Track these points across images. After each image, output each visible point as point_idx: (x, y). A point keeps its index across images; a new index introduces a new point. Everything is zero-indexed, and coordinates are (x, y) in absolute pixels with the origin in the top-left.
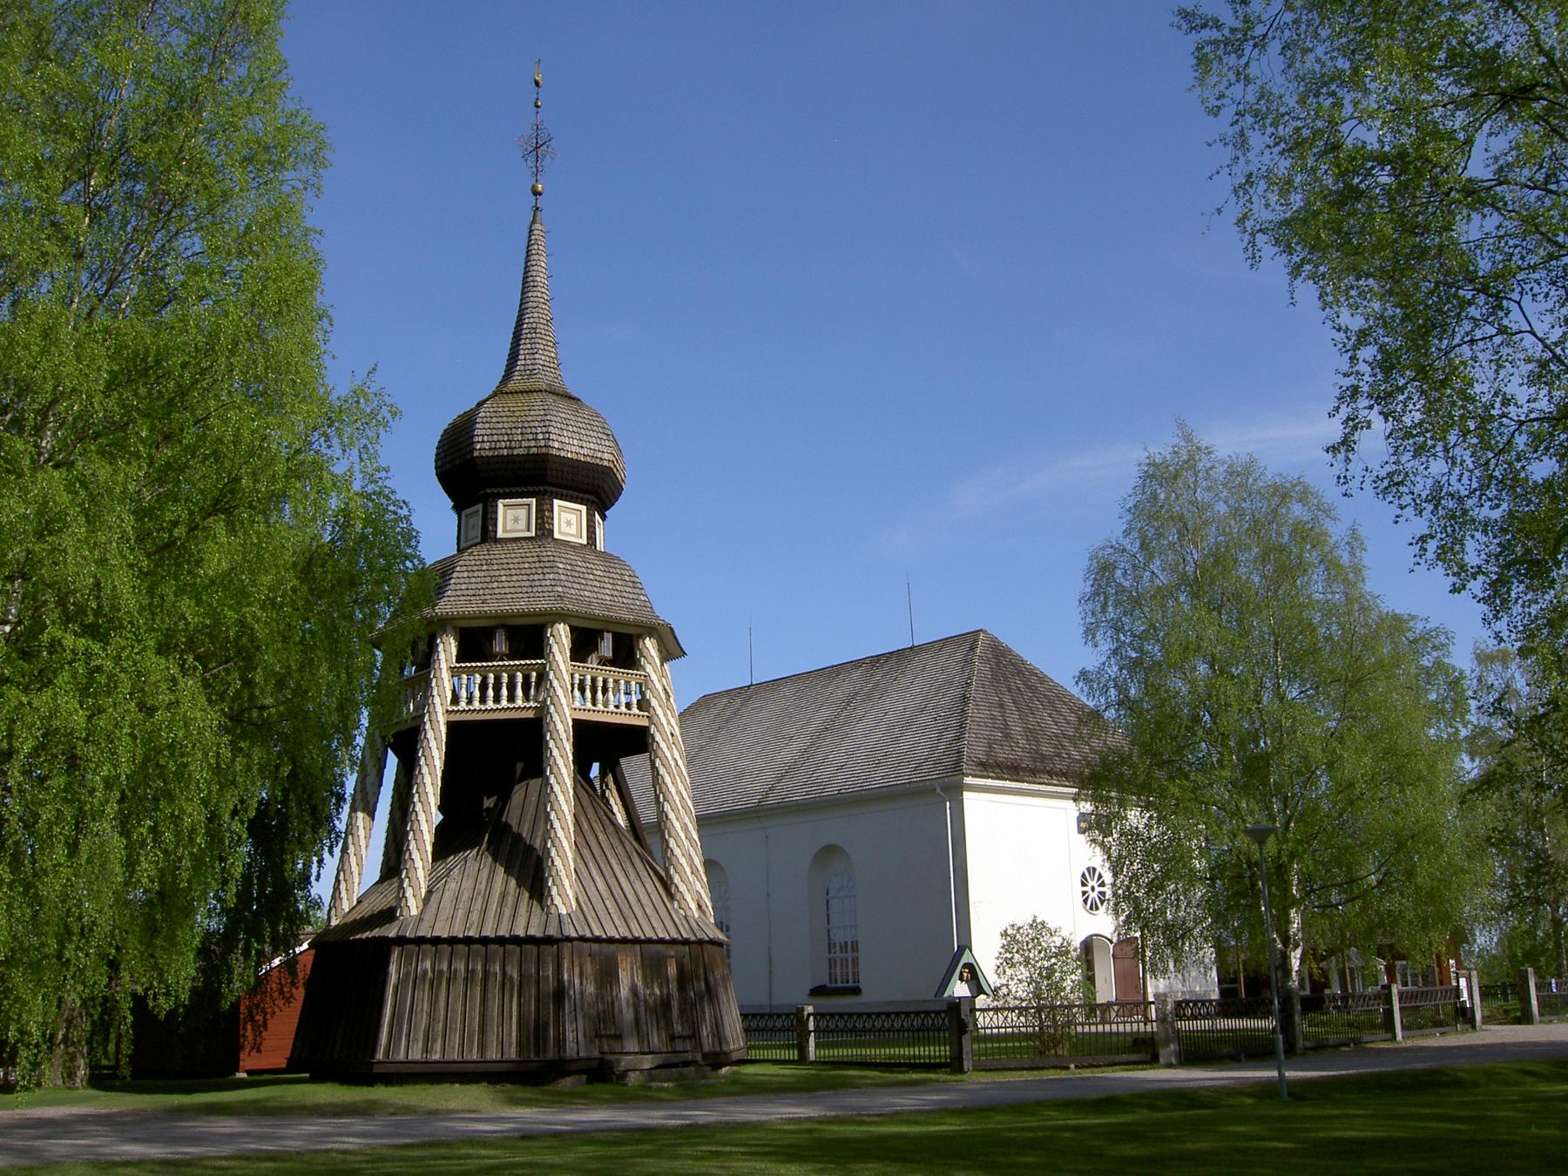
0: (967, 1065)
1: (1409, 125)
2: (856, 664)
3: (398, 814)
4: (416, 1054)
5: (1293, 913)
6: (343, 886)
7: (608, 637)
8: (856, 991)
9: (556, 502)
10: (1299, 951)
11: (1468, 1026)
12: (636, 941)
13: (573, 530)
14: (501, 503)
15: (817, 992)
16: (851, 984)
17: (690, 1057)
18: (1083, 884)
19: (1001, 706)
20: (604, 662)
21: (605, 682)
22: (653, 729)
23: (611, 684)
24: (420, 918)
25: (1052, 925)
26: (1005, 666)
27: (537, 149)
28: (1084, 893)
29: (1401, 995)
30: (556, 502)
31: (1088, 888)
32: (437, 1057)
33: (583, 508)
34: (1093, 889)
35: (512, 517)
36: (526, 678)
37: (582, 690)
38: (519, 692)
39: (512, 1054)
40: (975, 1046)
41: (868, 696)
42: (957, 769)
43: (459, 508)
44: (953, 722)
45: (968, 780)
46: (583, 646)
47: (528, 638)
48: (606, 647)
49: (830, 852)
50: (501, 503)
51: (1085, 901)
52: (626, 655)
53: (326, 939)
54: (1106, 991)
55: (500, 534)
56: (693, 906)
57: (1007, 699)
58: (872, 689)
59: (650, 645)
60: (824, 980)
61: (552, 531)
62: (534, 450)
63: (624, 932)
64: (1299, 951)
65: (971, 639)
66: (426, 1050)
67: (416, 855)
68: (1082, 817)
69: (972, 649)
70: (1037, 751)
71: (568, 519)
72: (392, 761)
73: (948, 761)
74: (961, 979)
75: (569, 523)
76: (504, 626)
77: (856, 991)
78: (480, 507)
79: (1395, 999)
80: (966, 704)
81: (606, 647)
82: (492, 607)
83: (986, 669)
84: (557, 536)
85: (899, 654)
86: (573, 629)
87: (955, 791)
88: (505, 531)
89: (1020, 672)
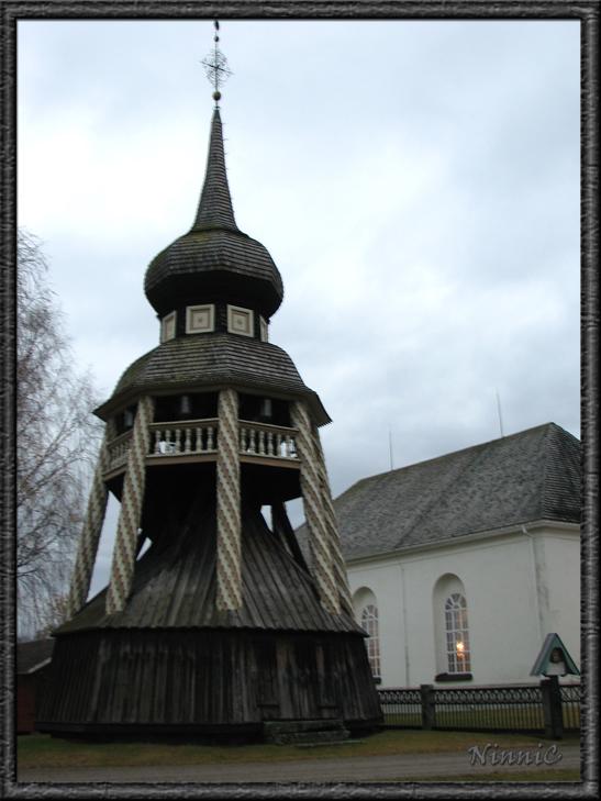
4: (116, 719)
9: (230, 307)
11: (125, 478)
12: (290, 632)
13: (243, 327)
14: (189, 309)
16: (465, 672)
17: (334, 722)
22: (304, 472)
27: (217, 97)
30: (230, 307)
32: (133, 720)
33: (251, 312)
35: (200, 319)
38: (199, 443)
43: (160, 317)
46: (248, 409)
47: (206, 405)
49: (448, 579)
50: (189, 309)
55: (188, 331)
56: (337, 606)
60: (445, 669)
61: (226, 328)
62: (212, 268)
63: (279, 624)
66: (125, 715)
67: (137, 489)
69: (545, 435)
71: (239, 321)
75: (240, 323)
76: (186, 394)
77: (469, 677)
78: (174, 313)
82: (179, 376)
84: (230, 330)
88: (192, 328)
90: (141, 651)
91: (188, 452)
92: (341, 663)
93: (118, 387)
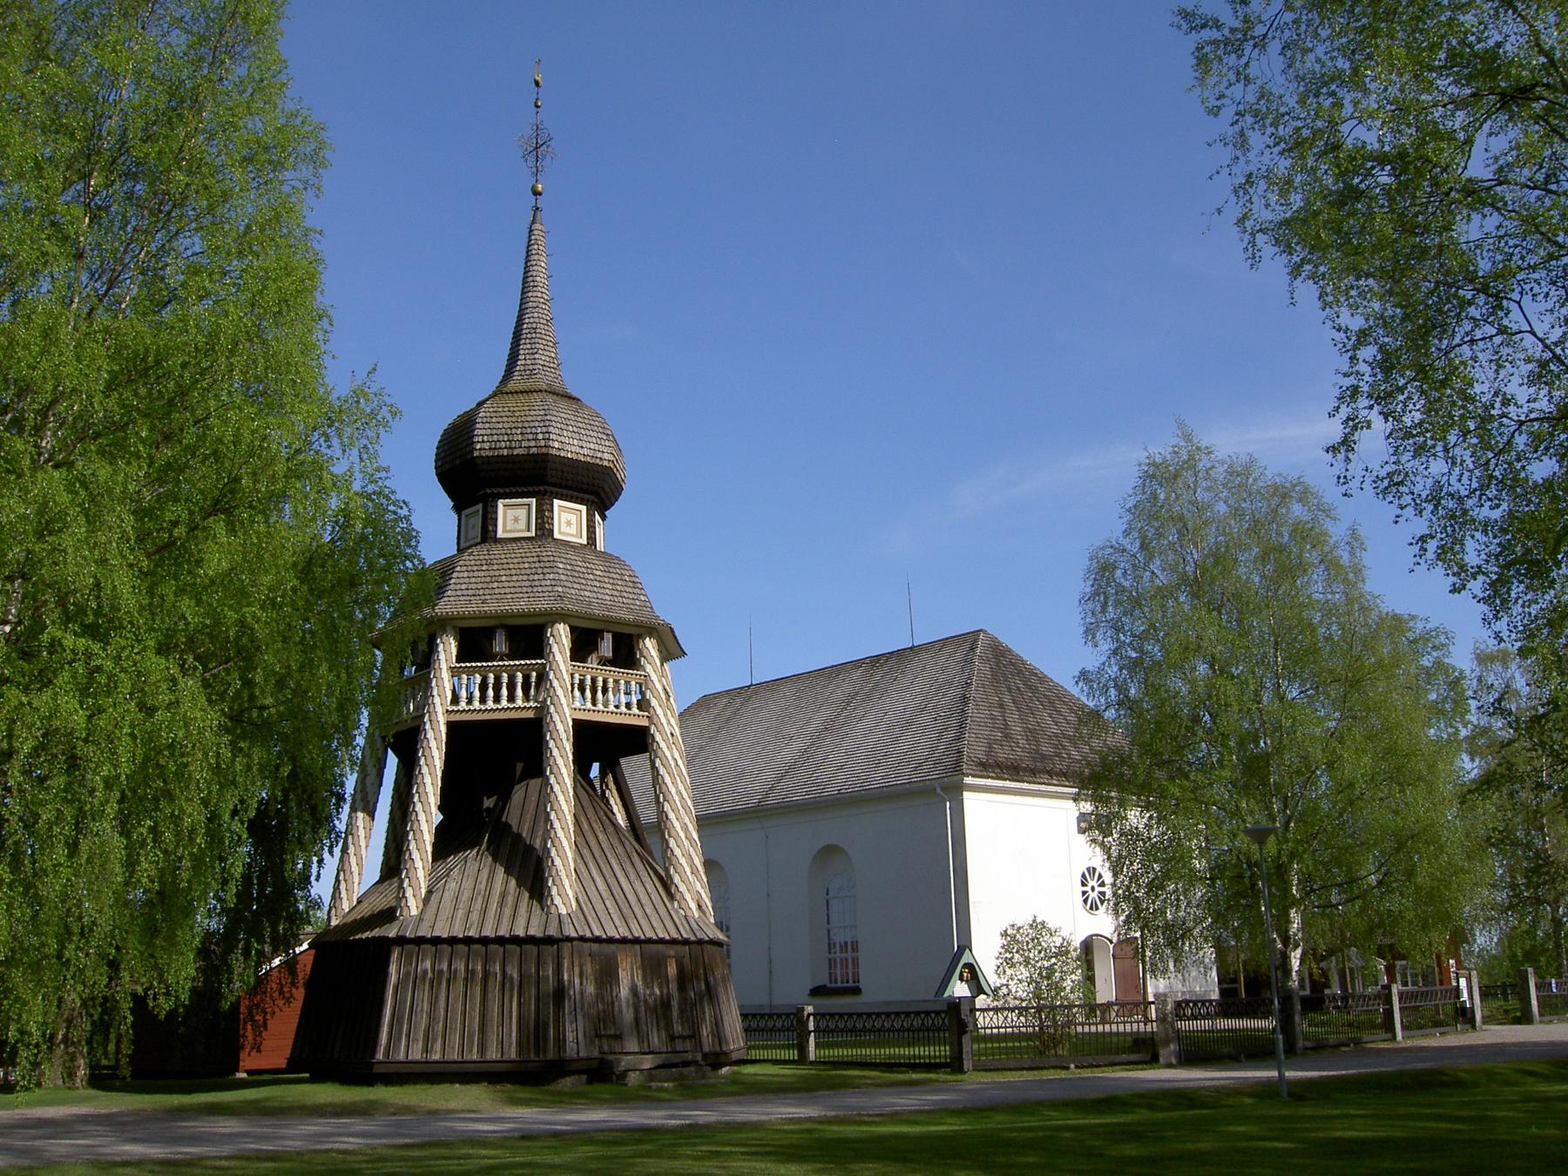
0: (967, 1065)
1: (1409, 125)
2: (856, 664)
3: (398, 814)
4: (416, 1054)
5: (1293, 913)
6: (343, 886)
7: (608, 637)
8: (856, 991)
9: (556, 502)
10: (1299, 951)
12: (636, 941)
13: (573, 530)
14: (501, 503)
15: (817, 992)
16: (851, 984)
18: (1083, 884)
19: (1001, 706)
20: (604, 662)
21: (605, 682)
22: (653, 729)
23: (611, 684)
24: (420, 918)
25: (1052, 925)
26: (1005, 666)
27: (537, 149)
28: (1084, 893)
29: (1401, 995)
30: (556, 502)
31: (1088, 888)
32: (437, 1057)
33: (583, 508)
34: (1093, 889)
35: (512, 517)
36: (526, 678)
37: (582, 690)
38: (519, 692)
39: (512, 1054)
40: (975, 1046)
41: (868, 696)
42: (957, 769)
43: (459, 508)
44: (953, 722)
45: (968, 780)
46: (583, 646)
47: (528, 638)
48: (606, 647)
49: (830, 852)
50: (501, 503)
51: (1085, 901)
52: (626, 655)
53: (326, 939)
54: (1106, 991)
55: (500, 534)
56: (693, 906)
57: (1007, 699)
58: (872, 689)
59: (650, 645)
60: (824, 980)
61: (552, 531)
62: (534, 450)
63: (624, 932)
64: (1299, 951)
65: (971, 639)
66: (426, 1050)
68: (1082, 817)
70: (1037, 751)
71: (568, 519)
72: (392, 761)
73: (948, 761)
74: (961, 979)
75: (569, 523)
76: (504, 626)
77: (856, 991)
78: (480, 507)
79: (1395, 999)
80: (966, 704)
81: (606, 647)
82: (492, 607)
83: (986, 669)
84: (557, 536)
85: (899, 654)
86: (573, 629)
87: (955, 791)
88: (505, 531)
89: (1020, 672)
90: (445, 967)
91: (490, 704)
92: (633, 1165)
93: (1483, 1046)
